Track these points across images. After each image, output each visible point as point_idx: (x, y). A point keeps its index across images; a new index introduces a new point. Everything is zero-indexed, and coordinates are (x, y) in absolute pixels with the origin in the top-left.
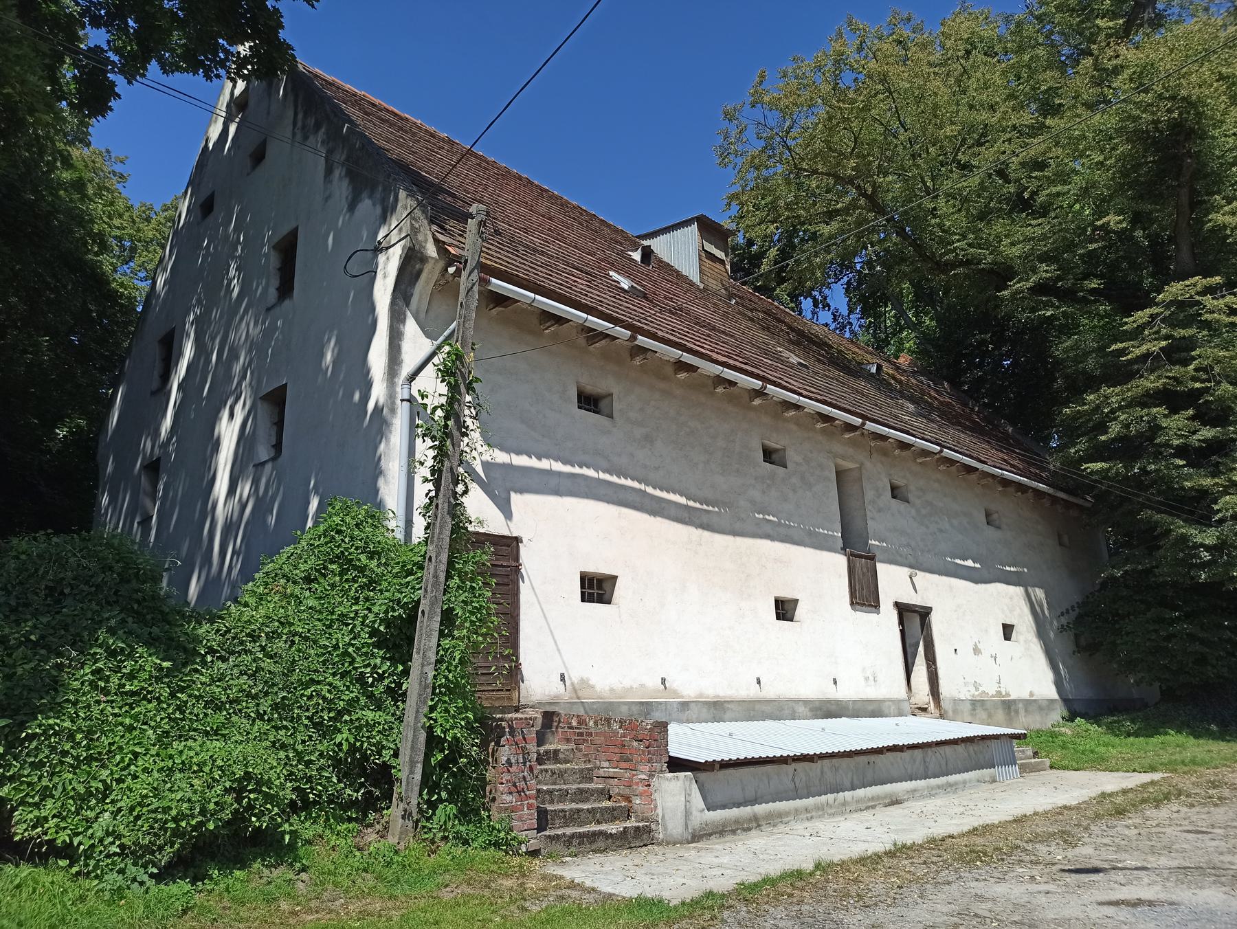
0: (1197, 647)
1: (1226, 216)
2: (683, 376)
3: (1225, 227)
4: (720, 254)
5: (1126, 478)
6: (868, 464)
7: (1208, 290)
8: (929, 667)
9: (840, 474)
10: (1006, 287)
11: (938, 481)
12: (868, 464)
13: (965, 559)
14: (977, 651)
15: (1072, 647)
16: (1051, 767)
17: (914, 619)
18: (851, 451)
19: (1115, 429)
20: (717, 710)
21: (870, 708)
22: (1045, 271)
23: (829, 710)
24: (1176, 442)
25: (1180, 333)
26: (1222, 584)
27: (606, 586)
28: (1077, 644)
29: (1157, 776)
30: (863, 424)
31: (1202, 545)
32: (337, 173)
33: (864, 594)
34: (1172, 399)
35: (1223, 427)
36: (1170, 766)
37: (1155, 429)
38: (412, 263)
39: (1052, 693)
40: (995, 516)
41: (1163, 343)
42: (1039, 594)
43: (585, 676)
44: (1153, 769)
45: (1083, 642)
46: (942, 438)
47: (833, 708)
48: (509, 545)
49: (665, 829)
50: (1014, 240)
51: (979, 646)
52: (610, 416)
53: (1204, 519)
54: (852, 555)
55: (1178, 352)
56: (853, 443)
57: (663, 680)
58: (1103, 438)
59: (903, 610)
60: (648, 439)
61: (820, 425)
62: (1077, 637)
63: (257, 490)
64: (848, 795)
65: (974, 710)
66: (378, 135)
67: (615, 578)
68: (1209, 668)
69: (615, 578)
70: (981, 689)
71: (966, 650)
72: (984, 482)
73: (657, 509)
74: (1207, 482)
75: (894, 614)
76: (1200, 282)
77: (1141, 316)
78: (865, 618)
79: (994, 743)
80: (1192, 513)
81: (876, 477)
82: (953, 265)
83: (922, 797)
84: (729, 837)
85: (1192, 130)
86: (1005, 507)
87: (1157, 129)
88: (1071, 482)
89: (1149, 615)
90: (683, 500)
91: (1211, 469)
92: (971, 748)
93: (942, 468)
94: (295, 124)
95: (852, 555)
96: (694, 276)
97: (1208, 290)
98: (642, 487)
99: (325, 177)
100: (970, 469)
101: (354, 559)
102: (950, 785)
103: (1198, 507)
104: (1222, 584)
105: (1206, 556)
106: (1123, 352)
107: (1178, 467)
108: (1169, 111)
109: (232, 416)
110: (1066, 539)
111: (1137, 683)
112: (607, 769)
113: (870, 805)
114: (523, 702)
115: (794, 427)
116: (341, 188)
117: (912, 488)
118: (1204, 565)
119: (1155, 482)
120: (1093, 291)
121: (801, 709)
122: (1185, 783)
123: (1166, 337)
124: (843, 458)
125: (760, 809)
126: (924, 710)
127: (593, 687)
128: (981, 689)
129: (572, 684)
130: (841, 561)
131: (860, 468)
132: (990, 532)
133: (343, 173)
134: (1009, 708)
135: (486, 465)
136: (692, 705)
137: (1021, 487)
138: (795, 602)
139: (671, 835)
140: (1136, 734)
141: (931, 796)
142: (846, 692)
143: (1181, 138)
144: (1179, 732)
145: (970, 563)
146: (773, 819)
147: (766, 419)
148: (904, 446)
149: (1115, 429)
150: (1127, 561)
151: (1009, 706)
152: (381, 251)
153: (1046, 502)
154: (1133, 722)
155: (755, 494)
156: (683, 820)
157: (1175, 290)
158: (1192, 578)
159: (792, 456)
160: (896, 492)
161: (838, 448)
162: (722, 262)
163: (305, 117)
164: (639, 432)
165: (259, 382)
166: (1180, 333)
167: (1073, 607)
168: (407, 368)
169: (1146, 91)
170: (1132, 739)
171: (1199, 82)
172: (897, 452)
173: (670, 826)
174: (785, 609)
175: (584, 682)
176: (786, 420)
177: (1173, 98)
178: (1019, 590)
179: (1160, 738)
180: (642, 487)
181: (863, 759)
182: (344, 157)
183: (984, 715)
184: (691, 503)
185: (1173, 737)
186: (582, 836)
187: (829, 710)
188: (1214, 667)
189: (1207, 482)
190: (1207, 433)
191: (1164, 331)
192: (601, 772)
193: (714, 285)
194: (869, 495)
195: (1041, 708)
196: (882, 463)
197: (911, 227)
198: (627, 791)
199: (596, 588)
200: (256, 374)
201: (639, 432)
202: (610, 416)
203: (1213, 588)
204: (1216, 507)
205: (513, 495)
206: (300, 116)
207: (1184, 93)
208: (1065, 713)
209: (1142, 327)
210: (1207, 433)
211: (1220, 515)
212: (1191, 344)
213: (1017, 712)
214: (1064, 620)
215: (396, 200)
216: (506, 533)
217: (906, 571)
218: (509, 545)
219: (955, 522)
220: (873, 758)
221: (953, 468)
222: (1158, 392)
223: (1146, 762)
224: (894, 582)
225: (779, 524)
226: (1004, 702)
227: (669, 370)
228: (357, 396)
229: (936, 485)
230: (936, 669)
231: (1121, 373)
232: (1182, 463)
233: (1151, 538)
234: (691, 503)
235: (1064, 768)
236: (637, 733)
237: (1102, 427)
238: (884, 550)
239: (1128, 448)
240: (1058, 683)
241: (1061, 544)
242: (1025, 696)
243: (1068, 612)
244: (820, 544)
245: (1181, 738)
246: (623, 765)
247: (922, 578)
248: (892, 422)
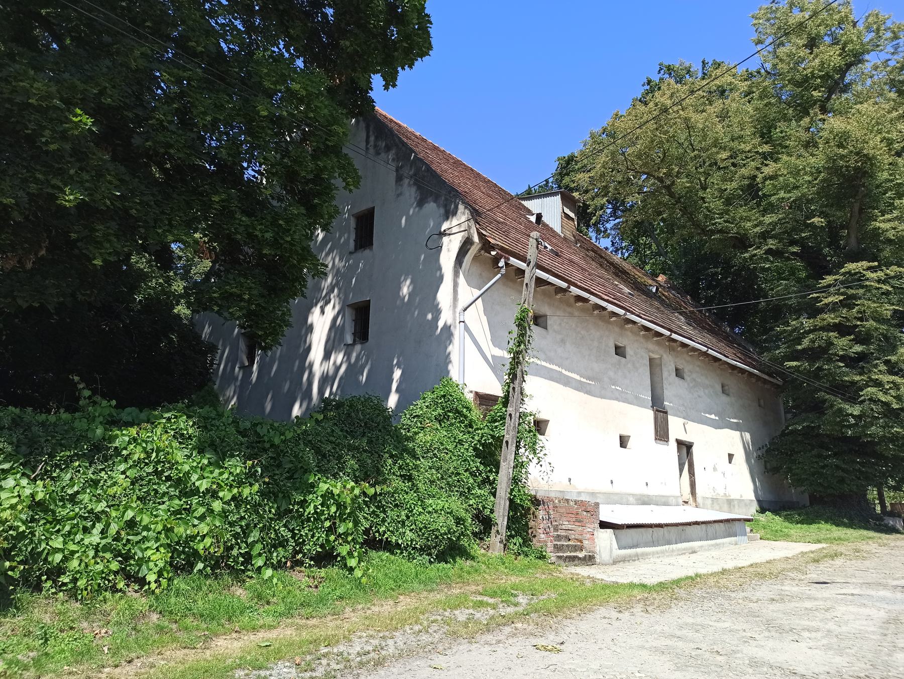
0: (840, 473)
1: (884, 224)
2: (579, 304)
3: (879, 228)
4: (572, 215)
5: (809, 371)
6: (665, 356)
7: (869, 268)
8: (690, 478)
9: (651, 360)
10: (747, 252)
11: (699, 366)
12: (665, 356)
13: (711, 414)
14: (715, 469)
17: (685, 447)
19: (806, 343)
21: (663, 500)
22: (772, 244)
23: (644, 501)
24: (841, 353)
25: (851, 292)
26: (860, 437)
27: (542, 426)
29: (820, 546)
30: (569, 287)
31: (851, 415)
32: (406, 181)
33: (662, 434)
34: (842, 329)
35: (867, 345)
36: (826, 540)
37: (830, 344)
38: (466, 244)
39: (751, 496)
40: (726, 388)
41: (842, 298)
42: (747, 436)
44: (819, 542)
45: (769, 467)
46: (707, 342)
47: (646, 499)
50: (751, 221)
52: (546, 328)
53: (853, 399)
54: (657, 410)
55: (848, 302)
56: (658, 344)
58: (799, 347)
59: (680, 443)
60: (563, 341)
61: (642, 333)
63: (349, 359)
64: (674, 546)
66: (440, 167)
67: (548, 421)
69: (548, 421)
71: (710, 469)
72: (722, 367)
73: (566, 382)
74: (857, 378)
76: (865, 264)
77: (829, 279)
78: (661, 447)
79: (737, 523)
80: (844, 395)
81: (669, 363)
82: (713, 232)
83: (705, 550)
84: (627, 563)
85: (866, 172)
86: (733, 383)
87: (847, 170)
88: (773, 370)
89: (813, 452)
90: (578, 377)
92: (727, 525)
93: (701, 358)
94: (367, 142)
95: (657, 410)
96: (557, 229)
97: (869, 268)
98: (560, 369)
99: (397, 182)
100: (716, 359)
101: (452, 410)
102: (717, 545)
103: (851, 393)
104: (860, 437)
105: (852, 421)
106: (817, 300)
107: (840, 367)
108: (857, 162)
109: (323, 312)
110: (762, 402)
112: (566, 525)
113: (682, 553)
115: (629, 333)
116: (410, 193)
117: (686, 370)
118: (850, 426)
119: (826, 375)
120: (793, 253)
121: (631, 499)
122: (841, 549)
123: (842, 294)
124: (653, 352)
125: (639, 550)
126: (686, 503)
130: (650, 414)
131: (661, 358)
132: (724, 398)
133: (412, 182)
135: (493, 356)
137: (742, 371)
138: (546, 422)
140: (802, 522)
141: (709, 550)
142: (652, 491)
143: (859, 175)
144: (826, 522)
145: (713, 416)
146: (644, 556)
147: (617, 329)
148: (684, 345)
149: (806, 343)
150: (804, 421)
152: (445, 235)
153: (754, 380)
154: (799, 515)
155: (611, 374)
157: (851, 266)
158: (843, 433)
159: (629, 351)
160: (679, 373)
161: (651, 346)
162: (572, 219)
163: (377, 138)
164: (559, 337)
165: (346, 296)
166: (851, 292)
168: (461, 304)
169: (844, 147)
170: (799, 525)
171: (874, 145)
173: (603, 556)
174: (623, 442)
176: (626, 330)
177: (857, 154)
178: (738, 433)
179: (816, 526)
180: (560, 369)
181: (680, 527)
182: (412, 173)
184: (582, 379)
185: (823, 526)
186: (570, 557)
187: (644, 501)
189: (857, 378)
190: (858, 348)
191: (842, 290)
192: (563, 527)
193: (569, 235)
194: (665, 374)
195: (746, 505)
197: (688, 204)
198: (580, 537)
200: (343, 291)
201: (559, 337)
202: (546, 328)
203: (854, 440)
204: (861, 393)
206: (372, 139)
207: (865, 152)
208: (758, 509)
209: (829, 286)
210: (858, 348)
211: (862, 398)
212: (855, 297)
214: (760, 453)
215: (456, 208)
217: (682, 421)
219: (707, 391)
220: (684, 527)
221: (745, 375)
222: (835, 325)
223: (815, 537)
224: (677, 427)
225: (622, 392)
226: (728, 500)
227: (572, 300)
228: (430, 316)
229: (698, 369)
231: (814, 311)
232: (842, 364)
233: (818, 407)
234: (582, 379)
235: (768, 539)
236: (584, 511)
237: (799, 341)
238: (672, 408)
239: (813, 354)
240: (756, 491)
241: (760, 406)
244: (639, 403)
245: (828, 526)
246: (577, 524)
247: (691, 425)
248: (681, 332)
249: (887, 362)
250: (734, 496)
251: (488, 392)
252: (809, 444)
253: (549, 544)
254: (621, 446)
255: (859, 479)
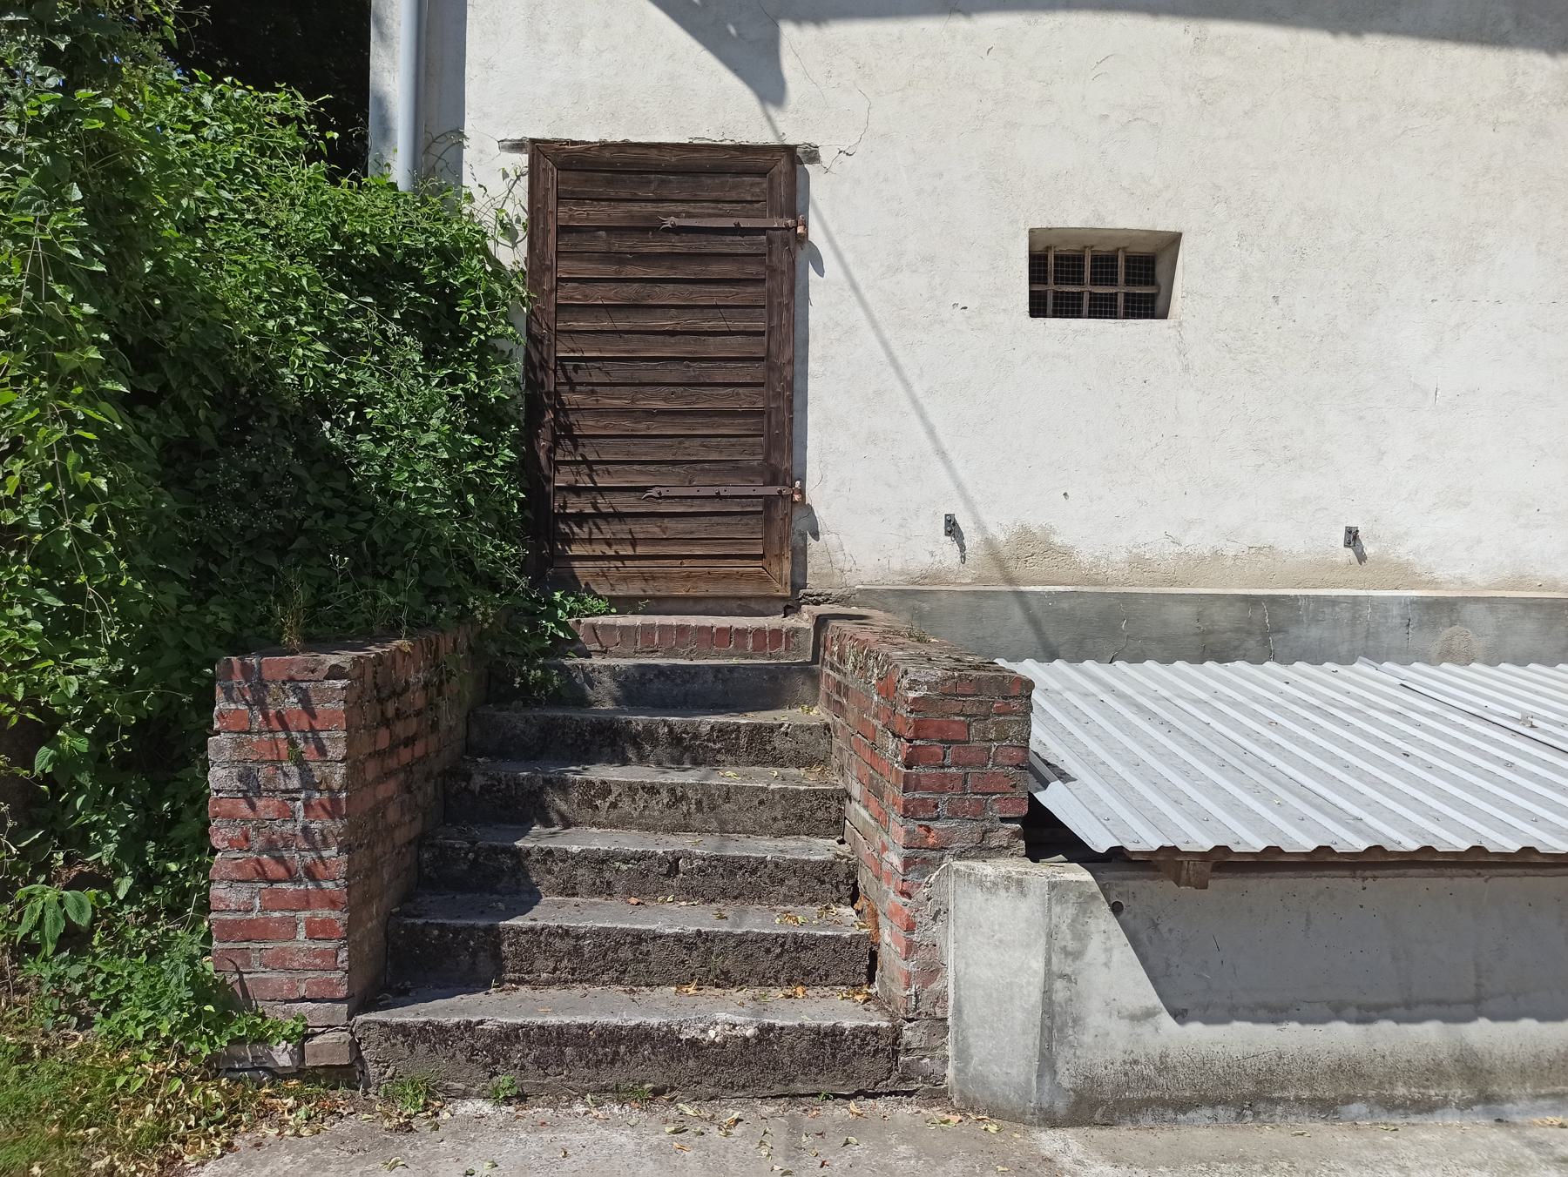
20: (1256, 627)
43: (1035, 522)
48: (776, 174)
49: (963, 1054)
57: (1352, 537)
69: (1174, 240)
114: (813, 585)
127: (1066, 552)
129: (989, 543)
136: (1468, 611)
139: (982, 1081)
156: (1032, 1040)
173: (980, 1048)
175: (1032, 542)
199: (1099, 277)
205: (788, 31)
216: (766, 137)
218: (776, 174)
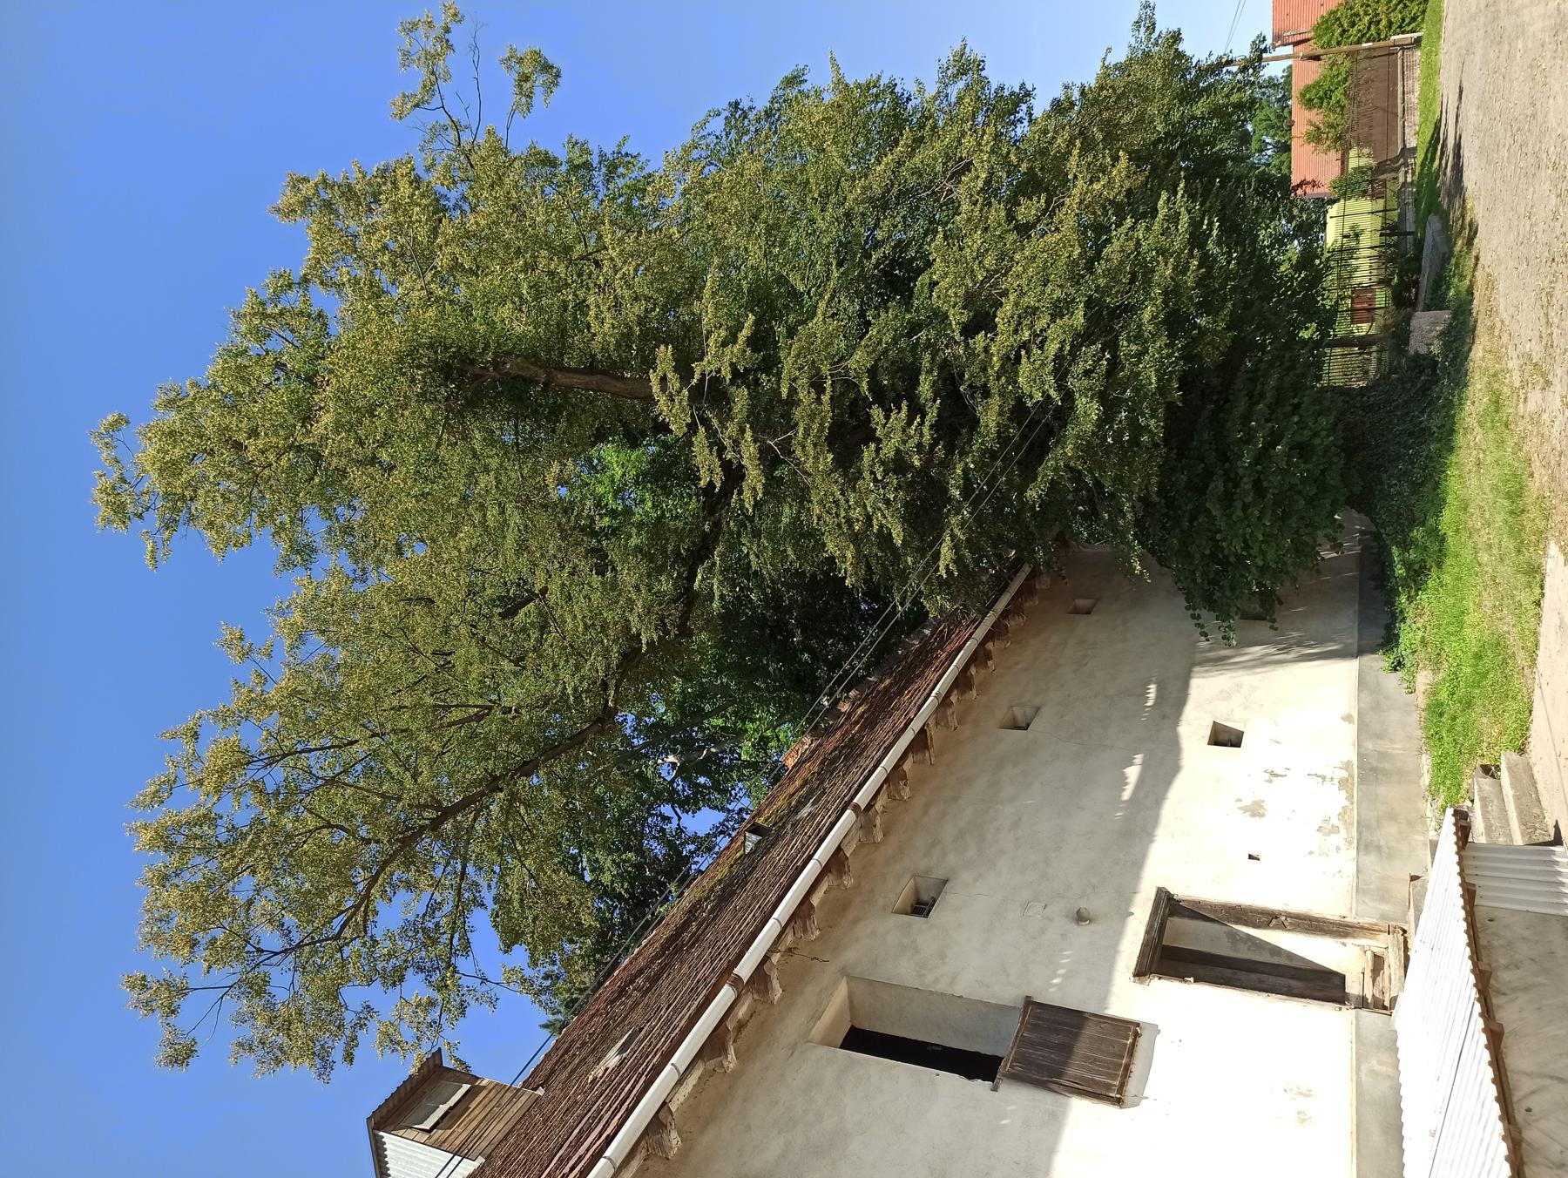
11: (927, 807)
12: (849, 956)
14: (1256, 810)
15: (1262, 629)
16: (1522, 750)
18: (810, 992)
21: (1376, 1137)
26: (1170, 407)
28: (1259, 618)
37: (899, 464)
40: (1018, 711)
41: (748, 435)
45: (1256, 607)
51: (1247, 802)
61: (731, 1061)
62: (1247, 616)
65: (1378, 848)
68: (1317, 441)
70: (1335, 821)
75: (1163, 988)
78: (1163, 1071)
86: (1008, 686)
89: (1216, 513)
91: (978, 395)
93: (906, 793)
104: (1170, 407)
111: (1337, 547)
117: (922, 864)
123: (742, 431)
128: (1335, 821)
134: (1374, 770)
151: (1371, 770)
161: (791, 1026)
167: (1193, 617)
172: (848, 881)
183: (1390, 829)
188: (1316, 435)
195: (1376, 707)
196: (857, 920)
213: (1383, 756)
226: (1363, 779)
229: (933, 811)
230: (1289, 915)
242: (1351, 731)
243: (1200, 626)
249: (969, 330)
250: (1342, 746)
251: (1161, 833)
252: (1193, 518)
253: (1267, 111)
254: (1237, 744)
255: (1296, 407)
